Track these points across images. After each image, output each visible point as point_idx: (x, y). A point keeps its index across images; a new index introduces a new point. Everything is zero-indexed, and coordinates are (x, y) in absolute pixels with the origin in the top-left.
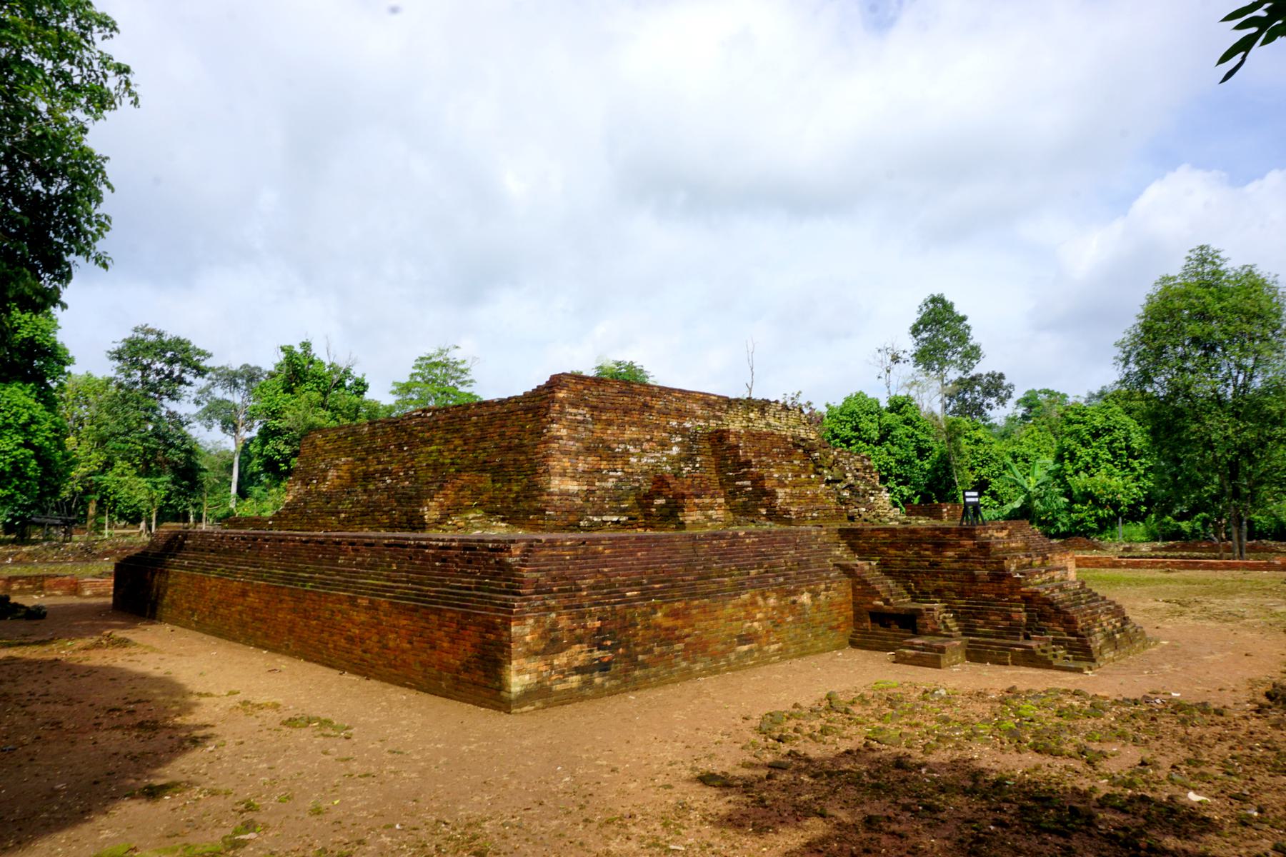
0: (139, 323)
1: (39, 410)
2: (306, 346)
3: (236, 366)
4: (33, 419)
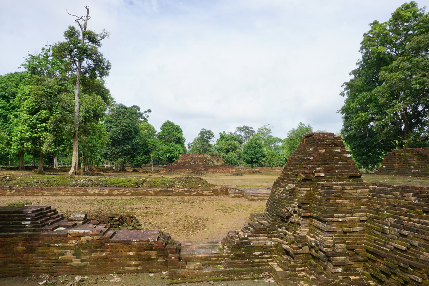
0: (202, 128)
1: (181, 148)
2: (224, 132)
3: (242, 126)
4: (180, 150)
